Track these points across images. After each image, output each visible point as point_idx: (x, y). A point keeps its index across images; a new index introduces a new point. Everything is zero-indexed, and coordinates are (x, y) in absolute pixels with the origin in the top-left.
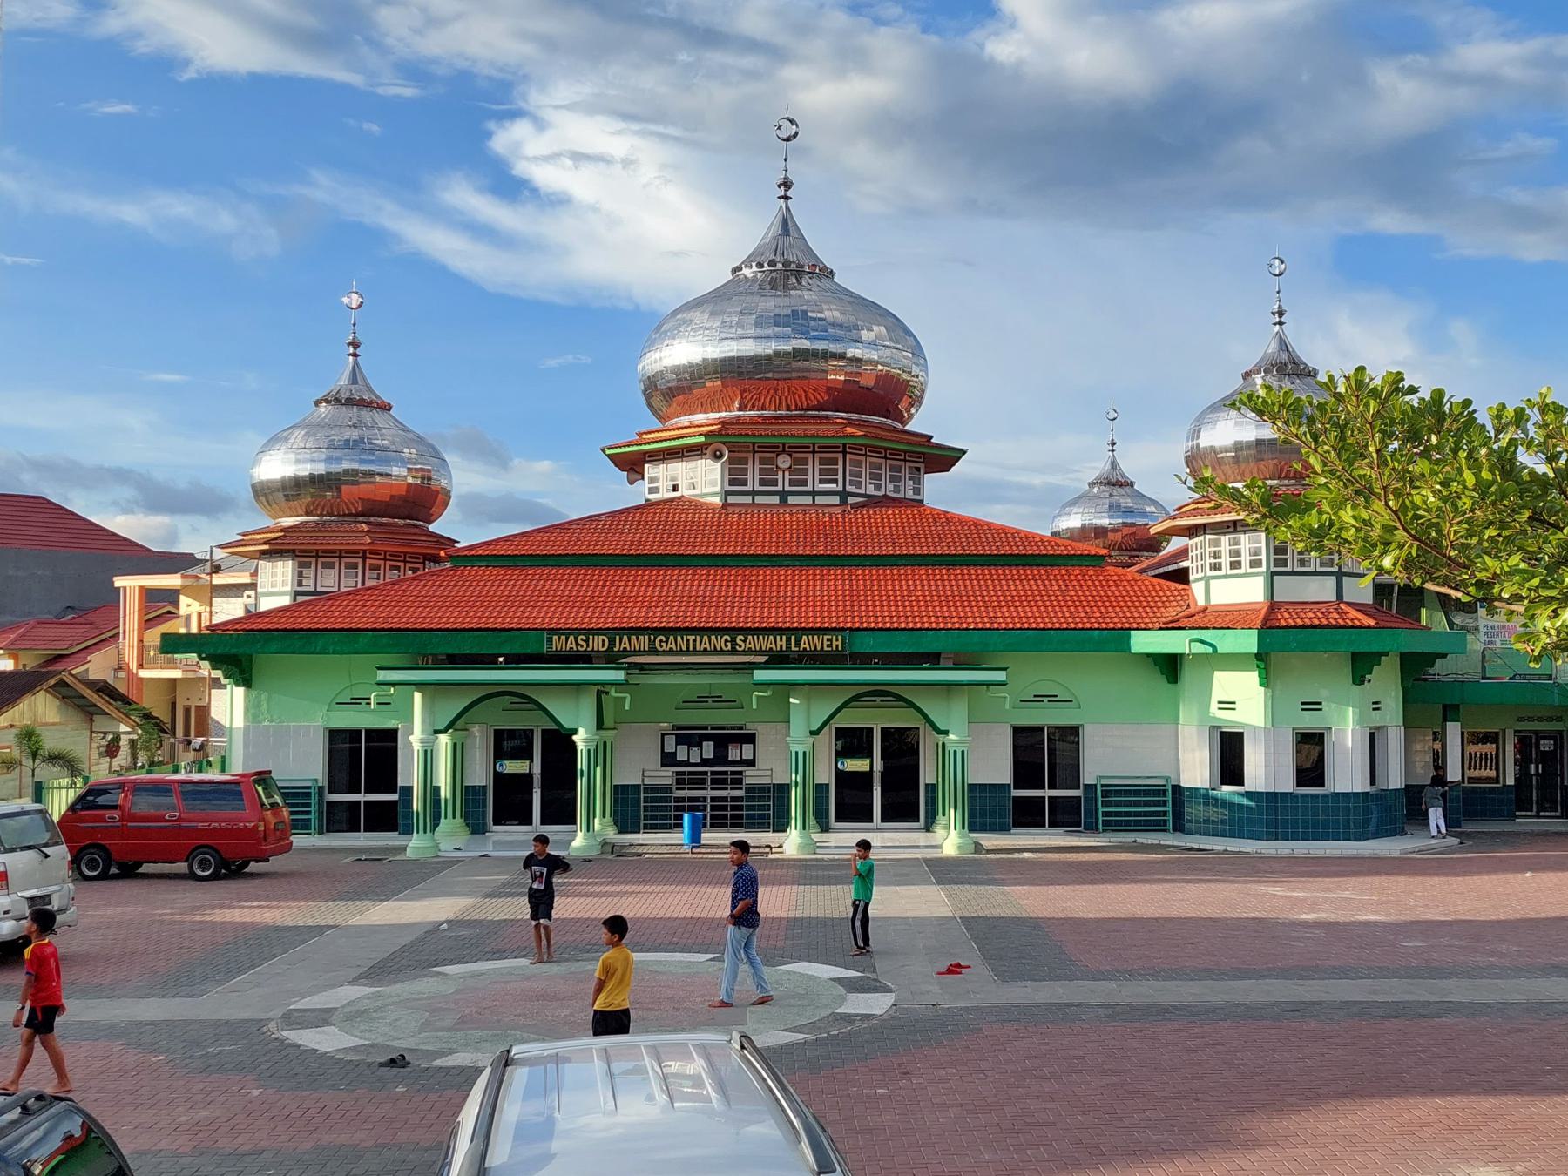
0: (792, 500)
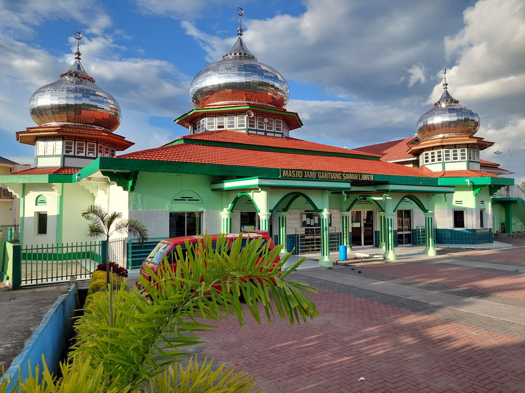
0: (268, 134)
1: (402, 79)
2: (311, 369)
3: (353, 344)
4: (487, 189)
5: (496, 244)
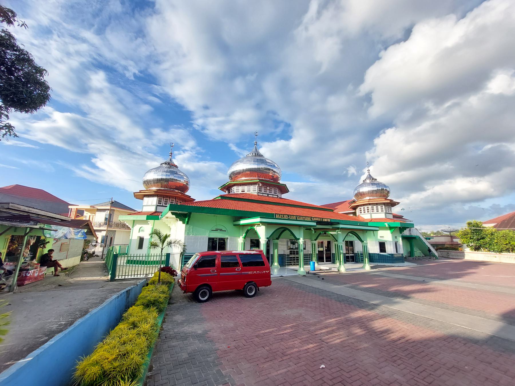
1: (345, 172)
2: (284, 354)
3: (317, 333)
4: (398, 229)
5: (406, 263)
